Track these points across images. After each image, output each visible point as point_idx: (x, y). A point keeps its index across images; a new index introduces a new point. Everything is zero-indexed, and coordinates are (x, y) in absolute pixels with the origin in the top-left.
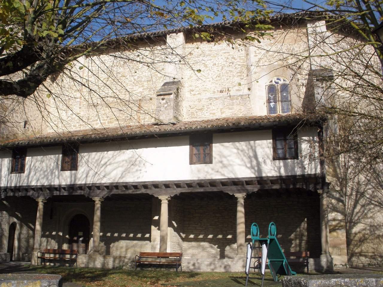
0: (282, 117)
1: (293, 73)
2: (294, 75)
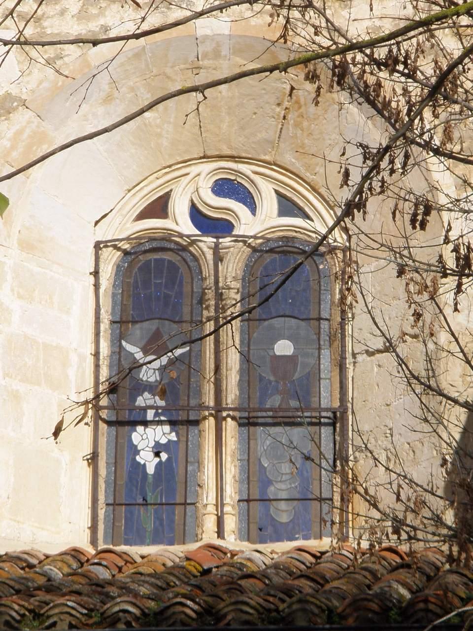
0: (238, 577)
1: (377, 134)
2: (375, 158)
